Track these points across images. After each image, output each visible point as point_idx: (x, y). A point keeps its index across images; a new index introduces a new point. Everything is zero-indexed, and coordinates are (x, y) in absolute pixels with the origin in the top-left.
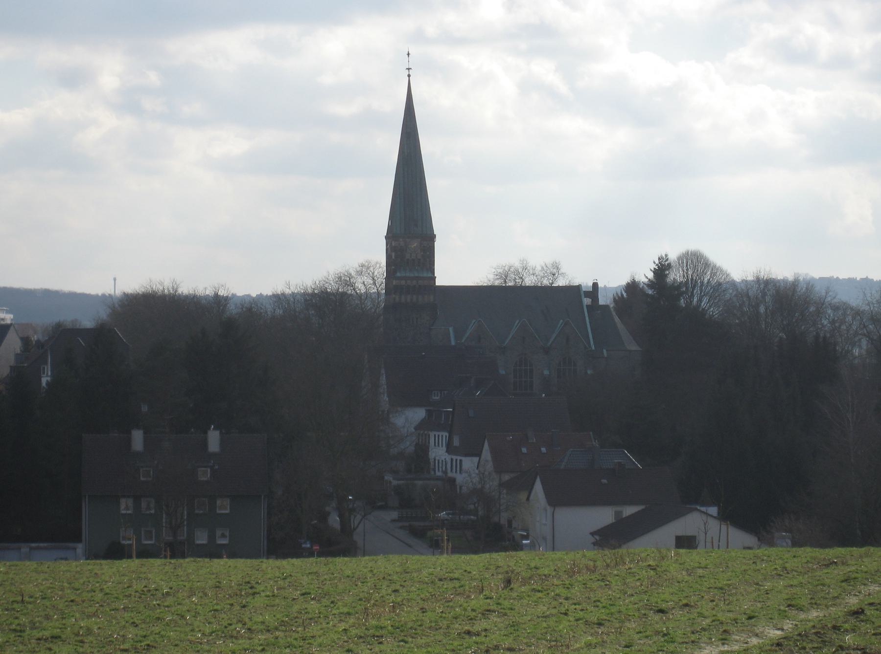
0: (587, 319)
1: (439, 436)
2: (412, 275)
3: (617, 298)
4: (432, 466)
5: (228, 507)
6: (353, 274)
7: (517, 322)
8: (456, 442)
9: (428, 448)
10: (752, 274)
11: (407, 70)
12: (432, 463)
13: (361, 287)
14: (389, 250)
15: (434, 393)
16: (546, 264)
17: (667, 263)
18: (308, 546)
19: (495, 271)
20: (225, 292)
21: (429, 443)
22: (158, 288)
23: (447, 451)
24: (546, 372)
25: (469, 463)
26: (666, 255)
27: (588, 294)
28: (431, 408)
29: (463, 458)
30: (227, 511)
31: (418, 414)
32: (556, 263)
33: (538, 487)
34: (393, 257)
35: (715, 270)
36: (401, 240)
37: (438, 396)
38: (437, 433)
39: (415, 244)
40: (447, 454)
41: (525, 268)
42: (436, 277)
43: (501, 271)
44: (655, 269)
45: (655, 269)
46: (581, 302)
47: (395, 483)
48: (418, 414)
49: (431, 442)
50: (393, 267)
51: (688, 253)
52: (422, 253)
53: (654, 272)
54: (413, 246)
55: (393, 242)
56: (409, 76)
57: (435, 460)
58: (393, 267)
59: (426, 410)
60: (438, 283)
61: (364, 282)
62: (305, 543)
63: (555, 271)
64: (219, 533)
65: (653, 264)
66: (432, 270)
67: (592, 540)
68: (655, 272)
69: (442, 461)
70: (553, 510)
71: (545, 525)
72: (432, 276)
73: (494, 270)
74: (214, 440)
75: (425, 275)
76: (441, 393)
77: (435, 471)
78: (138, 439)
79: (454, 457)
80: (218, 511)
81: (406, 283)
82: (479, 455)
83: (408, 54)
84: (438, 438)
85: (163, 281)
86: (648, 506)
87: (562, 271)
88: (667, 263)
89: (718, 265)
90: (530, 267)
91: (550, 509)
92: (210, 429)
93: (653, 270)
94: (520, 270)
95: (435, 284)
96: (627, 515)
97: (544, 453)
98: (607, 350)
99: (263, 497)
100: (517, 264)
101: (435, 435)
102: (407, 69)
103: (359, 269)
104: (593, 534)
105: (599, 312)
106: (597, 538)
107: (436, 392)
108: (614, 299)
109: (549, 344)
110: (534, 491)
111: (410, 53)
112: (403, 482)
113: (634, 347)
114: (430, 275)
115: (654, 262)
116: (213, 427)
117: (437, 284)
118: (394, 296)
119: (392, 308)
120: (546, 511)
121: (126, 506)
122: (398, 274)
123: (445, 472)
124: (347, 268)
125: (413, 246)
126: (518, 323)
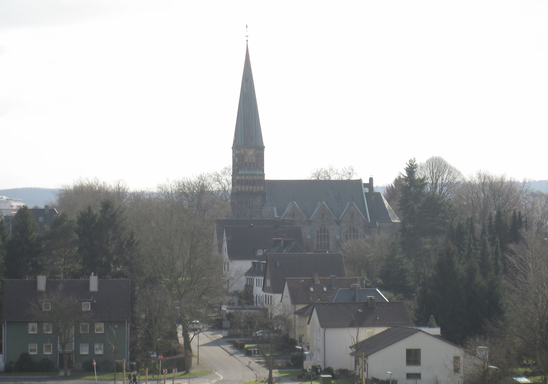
1: (259, 280)
2: (249, 173)
3: (389, 188)
4: (255, 300)
5: (103, 330)
6: (220, 174)
8: (268, 283)
9: (253, 287)
12: (255, 298)
13: (225, 182)
14: (234, 156)
15: (259, 251)
17: (415, 163)
18: (155, 355)
20: (124, 185)
22: (85, 182)
23: (263, 290)
24: (338, 237)
26: (414, 159)
27: (366, 185)
28: (256, 261)
29: (272, 295)
30: (103, 332)
32: (351, 166)
33: (315, 314)
34: (237, 161)
37: (261, 253)
38: (258, 278)
39: (251, 152)
40: (263, 292)
41: (331, 169)
44: (406, 168)
45: (406, 168)
46: (361, 190)
47: (228, 311)
48: (247, 265)
50: (237, 168)
51: (433, 158)
53: (406, 170)
54: (250, 154)
55: (237, 151)
56: (247, 41)
57: (257, 296)
58: (237, 168)
59: (252, 262)
60: (267, 178)
61: (227, 179)
62: (153, 354)
63: (350, 171)
64: (97, 346)
65: (406, 164)
66: (263, 170)
68: (407, 170)
69: (261, 297)
70: (324, 330)
71: (319, 341)
74: (94, 282)
75: (258, 173)
76: (263, 251)
77: (257, 303)
78: (42, 282)
79: (267, 294)
80: (96, 332)
81: (245, 178)
82: (281, 292)
84: (251, 280)
86: (389, 328)
88: (415, 163)
89: (453, 166)
91: (322, 330)
93: (406, 169)
94: (328, 171)
95: (264, 179)
97: (312, 292)
98: (379, 223)
99: (126, 322)
100: (327, 168)
101: (257, 279)
103: (223, 170)
104: (351, 347)
105: (374, 197)
107: (260, 250)
111: (246, 27)
112: (233, 311)
113: (396, 220)
114: (261, 173)
115: (406, 163)
116: (93, 274)
118: (237, 187)
119: (235, 194)
120: (320, 331)
121: (32, 328)
122: (240, 172)
123: (262, 304)
125: (250, 154)
126: (320, 204)
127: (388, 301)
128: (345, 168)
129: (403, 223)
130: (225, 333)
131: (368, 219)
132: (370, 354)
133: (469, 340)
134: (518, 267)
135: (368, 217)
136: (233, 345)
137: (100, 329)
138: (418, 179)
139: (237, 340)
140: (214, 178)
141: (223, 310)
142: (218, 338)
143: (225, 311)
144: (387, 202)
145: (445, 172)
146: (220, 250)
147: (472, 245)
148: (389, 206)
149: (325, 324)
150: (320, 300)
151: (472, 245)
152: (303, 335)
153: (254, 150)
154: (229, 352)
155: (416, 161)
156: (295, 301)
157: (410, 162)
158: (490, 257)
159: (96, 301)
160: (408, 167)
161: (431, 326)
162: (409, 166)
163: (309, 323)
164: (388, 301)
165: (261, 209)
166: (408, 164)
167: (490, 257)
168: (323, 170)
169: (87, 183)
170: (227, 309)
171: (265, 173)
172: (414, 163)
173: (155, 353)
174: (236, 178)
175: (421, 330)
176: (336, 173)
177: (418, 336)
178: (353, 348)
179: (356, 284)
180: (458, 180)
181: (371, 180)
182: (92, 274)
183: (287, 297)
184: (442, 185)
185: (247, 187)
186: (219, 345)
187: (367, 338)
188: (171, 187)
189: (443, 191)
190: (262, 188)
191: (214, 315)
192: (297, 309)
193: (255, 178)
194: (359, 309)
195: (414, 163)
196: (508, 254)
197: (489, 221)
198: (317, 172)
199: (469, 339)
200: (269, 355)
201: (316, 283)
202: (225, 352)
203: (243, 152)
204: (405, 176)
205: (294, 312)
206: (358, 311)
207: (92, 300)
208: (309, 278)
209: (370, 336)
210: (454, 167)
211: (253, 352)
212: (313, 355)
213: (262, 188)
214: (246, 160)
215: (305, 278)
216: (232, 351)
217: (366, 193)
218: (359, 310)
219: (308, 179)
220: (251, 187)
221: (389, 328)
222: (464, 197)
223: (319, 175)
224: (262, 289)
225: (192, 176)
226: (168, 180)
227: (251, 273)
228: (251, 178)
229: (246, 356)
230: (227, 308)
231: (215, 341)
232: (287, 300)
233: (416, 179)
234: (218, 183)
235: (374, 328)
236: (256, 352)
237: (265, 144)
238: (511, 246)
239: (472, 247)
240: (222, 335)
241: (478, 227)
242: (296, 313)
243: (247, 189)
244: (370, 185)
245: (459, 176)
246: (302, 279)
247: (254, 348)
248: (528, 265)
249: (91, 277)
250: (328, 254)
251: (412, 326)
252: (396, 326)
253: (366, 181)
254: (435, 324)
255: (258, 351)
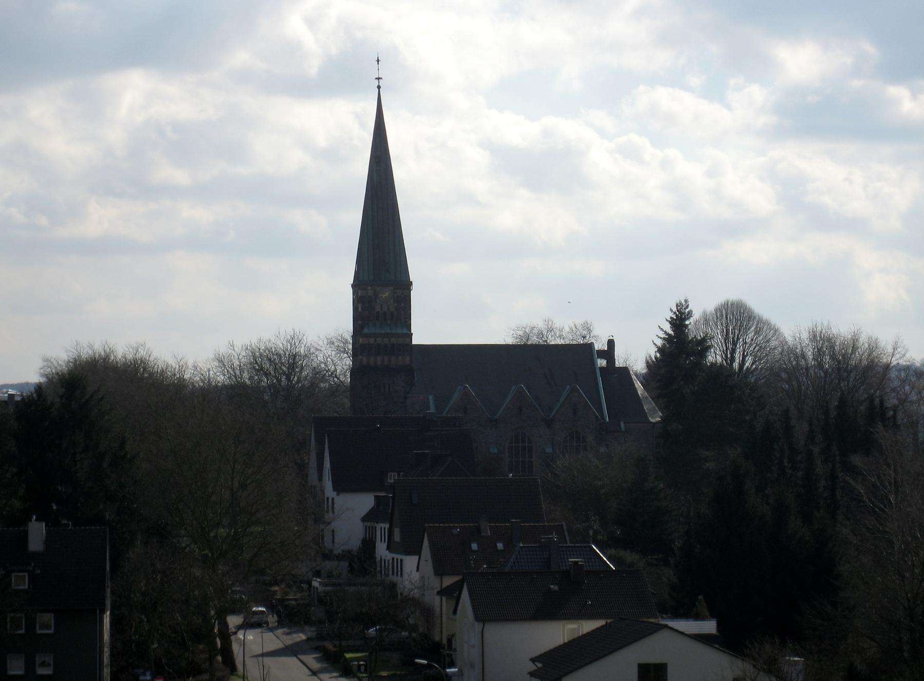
0: (600, 379)
2: (383, 332)
7: (513, 388)
8: (397, 537)
10: (807, 329)
11: (377, 81)
12: (378, 564)
16: (575, 325)
17: (687, 310)
19: (514, 332)
21: (376, 538)
22: (86, 353)
23: (388, 548)
24: (549, 450)
25: (410, 562)
26: (686, 301)
27: (601, 354)
29: (403, 557)
30: (51, 631)
31: (364, 502)
34: (360, 309)
35: (762, 326)
36: (369, 288)
39: (386, 294)
40: (388, 551)
41: (550, 330)
42: (412, 334)
43: (521, 333)
44: (671, 318)
45: (671, 318)
46: (593, 364)
48: (364, 502)
49: (377, 538)
50: (360, 322)
52: (396, 304)
53: (670, 322)
54: (384, 296)
56: (379, 87)
57: (381, 559)
58: (360, 322)
60: (416, 341)
62: (144, 674)
63: (585, 332)
64: (39, 659)
67: (532, 667)
71: (473, 646)
72: (408, 332)
73: (512, 332)
75: (399, 331)
79: (396, 556)
80: (39, 632)
81: (375, 340)
82: (418, 552)
83: (378, 61)
85: (93, 344)
86: (609, 621)
87: (594, 333)
88: (687, 310)
89: (781, 331)
90: (556, 328)
91: (478, 626)
92: (31, 520)
94: (545, 333)
96: (584, 633)
100: (541, 325)
101: (381, 528)
102: (376, 78)
104: (533, 660)
105: (616, 375)
106: (540, 665)
107: (393, 474)
108: (647, 362)
109: (553, 414)
110: (461, 601)
114: (405, 331)
115: (671, 310)
117: (413, 343)
118: (361, 357)
122: (366, 331)
124: (341, 331)
125: (384, 296)
126: (515, 388)
127: (614, 569)
128: (576, 327)
129: (664, 420)
130: (311, 632)
131: (605, 416)
132: (567, 674)
133: (750, 649)
134: (867, 501)
135: (604, 413)
136: (322, 654)
137: (46, 626)
138: (693, 339)
139: (329, 646)
140: (338, 346)
141: (314, 586)
142: (298, 640)
143: (317, 587)
144: (640, 385)
145: (749, 329)
146: (320, 478)
147: (786, 461)
148: (644, 393)
149: (483, 615)
150: (487, 567)
151: (786, 461)
152: (453, 635)
153: (392, 288)
154: (311, 667)
155: (690, 306)
156: (440, 570)
157: (677, 308)
158: (822, 484)
159: (39, 571)
160: (675, 318)
161: (698, 617)
162: (677, 316)
163: (455, 612)
164: (614, 569)
165: (405, 398)
166: (674, 311)
167: (822, 484)
168: (535, 331)
169: (91, 353)
170: (320, 584)
171: (412, 332)
172: (685, 309)
173: (148, 673)
174: (359, 341)
175: (666, 626)
176: (559, 336)
177: (660, 638)
178: (536, 661)
179: (552, 535)
180: (773, 343)
181: (611, 343)
182: (33, 517)
183: (427, 561)
184: (744, 353)
185: (379, 359)
186: (296, 656)
187: (566, 641)
188: (238, 359)
189: (747, 364)
190: (408, 360)
191: (298, 596)
192: (445, 585)
193: (394, 340)
194: (552, 584)
195: (685, 309)
196: (848, 475)
197: (823, 417)
198: (524, 334)
199: (750, 646)
200: (386, 675)
201: (482, 534)
202: (305, 668)
203: (371, 293)
204: (668, 334)
205: (439, 589)
206: (549, 588)
207: (31, 569)
208: (471, 525)
209: (571, 638)
210: (766, 320)
211: (355, 668)
212: (463, 674)
213: (408, 360)
214: (378, 309)
215: (463, 525)
216: (316, 665)
217: (602, 368)
218: (552, 586)
219: (504, 344)
220: (386, 358)
221: (609, 621)
222: (784, 375)
223: (528, 340)
224: (386, 548)
225: (278, 337)
226: (233, 346)
227: (370, 517)
228: (386, 341)
229: (341, 676)
230: (320, 583)
231: (292, 645)
232: (428, 567)
233: (690, 338)
234: (346, 355)
235: (579, 621)
236: (362, 668)
237: (413, 275)
238: (857, 460)
239: (786, 464)
240: (306, 635)
241: (801, 429)
242: (442, 592)
243: (379, 363)
244: (609, 353)
245: (775, 336)
246: (457, 527)
247: (358, 659)
248: (887, 497)
249: (30, 524)
250: (510, 479)
251: (656, 617)
252: (623, 617)
253: (600, 345)
254: (707, 613)
255: (365, 666)
